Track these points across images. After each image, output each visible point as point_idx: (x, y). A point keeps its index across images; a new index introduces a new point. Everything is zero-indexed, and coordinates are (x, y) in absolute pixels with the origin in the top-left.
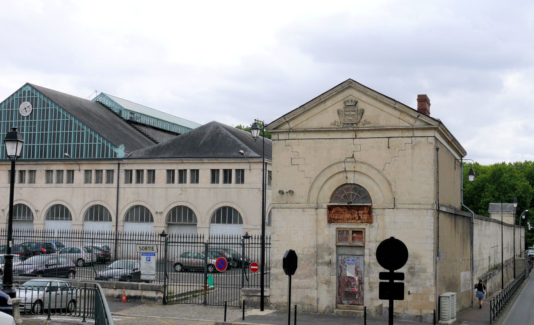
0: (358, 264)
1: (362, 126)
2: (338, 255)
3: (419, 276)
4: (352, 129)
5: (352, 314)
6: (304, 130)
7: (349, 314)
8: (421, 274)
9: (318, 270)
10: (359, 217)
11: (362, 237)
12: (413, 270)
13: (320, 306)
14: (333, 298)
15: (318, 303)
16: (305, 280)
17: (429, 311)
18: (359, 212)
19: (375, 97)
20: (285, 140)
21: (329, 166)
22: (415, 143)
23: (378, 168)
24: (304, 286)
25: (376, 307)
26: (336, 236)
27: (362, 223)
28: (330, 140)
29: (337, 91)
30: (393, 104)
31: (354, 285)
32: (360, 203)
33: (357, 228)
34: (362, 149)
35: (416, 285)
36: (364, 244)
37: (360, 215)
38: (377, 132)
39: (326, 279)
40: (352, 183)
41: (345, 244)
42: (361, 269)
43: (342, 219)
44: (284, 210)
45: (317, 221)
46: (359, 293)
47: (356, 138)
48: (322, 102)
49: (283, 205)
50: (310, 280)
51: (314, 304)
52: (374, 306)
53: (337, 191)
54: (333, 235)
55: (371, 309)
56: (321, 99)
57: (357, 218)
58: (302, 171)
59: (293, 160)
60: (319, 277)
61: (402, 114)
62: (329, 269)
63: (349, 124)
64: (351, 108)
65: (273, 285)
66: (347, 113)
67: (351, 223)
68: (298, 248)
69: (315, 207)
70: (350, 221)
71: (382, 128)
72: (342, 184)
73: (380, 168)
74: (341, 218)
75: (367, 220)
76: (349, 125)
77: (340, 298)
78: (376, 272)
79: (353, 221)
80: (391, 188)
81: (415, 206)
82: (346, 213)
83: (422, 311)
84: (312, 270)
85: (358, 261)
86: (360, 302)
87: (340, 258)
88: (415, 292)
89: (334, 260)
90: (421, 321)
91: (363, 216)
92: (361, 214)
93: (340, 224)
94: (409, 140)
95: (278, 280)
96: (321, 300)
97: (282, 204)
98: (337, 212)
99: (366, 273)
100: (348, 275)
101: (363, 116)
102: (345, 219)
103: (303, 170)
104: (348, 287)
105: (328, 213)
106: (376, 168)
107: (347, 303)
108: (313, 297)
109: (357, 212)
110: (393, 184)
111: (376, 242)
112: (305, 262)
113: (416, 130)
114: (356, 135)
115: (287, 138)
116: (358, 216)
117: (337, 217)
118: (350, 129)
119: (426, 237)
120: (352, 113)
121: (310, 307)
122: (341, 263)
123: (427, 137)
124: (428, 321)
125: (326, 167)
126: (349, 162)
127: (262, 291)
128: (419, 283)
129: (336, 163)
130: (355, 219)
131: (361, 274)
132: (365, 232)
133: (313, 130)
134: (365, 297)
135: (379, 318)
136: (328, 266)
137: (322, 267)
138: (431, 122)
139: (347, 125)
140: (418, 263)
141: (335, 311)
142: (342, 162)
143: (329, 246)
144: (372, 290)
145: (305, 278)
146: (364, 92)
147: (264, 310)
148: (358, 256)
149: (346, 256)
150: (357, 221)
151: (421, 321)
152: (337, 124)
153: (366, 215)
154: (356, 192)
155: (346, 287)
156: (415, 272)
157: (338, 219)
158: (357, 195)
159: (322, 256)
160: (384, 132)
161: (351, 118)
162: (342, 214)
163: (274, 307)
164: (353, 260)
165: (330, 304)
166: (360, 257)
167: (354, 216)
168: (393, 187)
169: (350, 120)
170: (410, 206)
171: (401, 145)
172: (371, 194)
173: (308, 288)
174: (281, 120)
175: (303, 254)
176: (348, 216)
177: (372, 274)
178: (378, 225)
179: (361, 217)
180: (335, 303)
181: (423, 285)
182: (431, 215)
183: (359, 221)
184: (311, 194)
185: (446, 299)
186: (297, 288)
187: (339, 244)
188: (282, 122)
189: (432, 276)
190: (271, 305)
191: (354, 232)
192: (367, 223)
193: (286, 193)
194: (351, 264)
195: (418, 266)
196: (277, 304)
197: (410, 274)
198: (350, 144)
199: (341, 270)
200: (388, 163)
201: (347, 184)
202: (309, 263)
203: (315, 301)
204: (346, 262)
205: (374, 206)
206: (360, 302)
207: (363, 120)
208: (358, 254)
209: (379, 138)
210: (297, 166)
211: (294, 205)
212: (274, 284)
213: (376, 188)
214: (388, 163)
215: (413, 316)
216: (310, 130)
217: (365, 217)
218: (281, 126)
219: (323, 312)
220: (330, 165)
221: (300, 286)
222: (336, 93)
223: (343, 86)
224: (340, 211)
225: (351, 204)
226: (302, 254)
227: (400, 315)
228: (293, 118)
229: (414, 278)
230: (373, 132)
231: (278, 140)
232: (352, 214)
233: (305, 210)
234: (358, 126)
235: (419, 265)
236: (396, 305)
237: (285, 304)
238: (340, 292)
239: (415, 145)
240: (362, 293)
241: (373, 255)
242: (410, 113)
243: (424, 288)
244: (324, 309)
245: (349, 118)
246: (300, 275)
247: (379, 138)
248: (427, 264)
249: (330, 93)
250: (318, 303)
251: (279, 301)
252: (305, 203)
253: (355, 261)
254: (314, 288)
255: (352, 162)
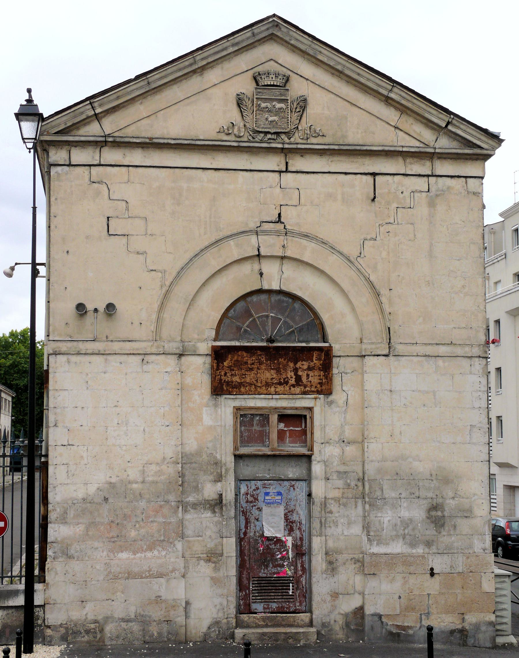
0: (293, 503)
1: (305, 142)
2: (239, 480)
3: (455, 527)
4: (280, 146)
5: (285, 640)
6: (148, 141)
7: (277, 640)
8: (460, 522)
9: (186, 523)
10: (298, 379)
11: (304, 432)
12: (439, 513)
13: (192, 622)
14: (229, 598)
15: (187, 617)
16: (149, 554)
17: (482, 615)
18: (299, 365)
19: (339, 67)
20: (90, 166)
21: (217, 242)
22: (437, 191)
23: (345, 250)
24: (149, 571)
25: (346, 615)
26: (235, 430)
27: (305, 393)
28: (217, 172)
29: (237, 44)
30: (386, 89)
31: (283, 558)
32: (295, 341)
33: (291, 408)
34: (302, 201)
35: (448, 551)
36: (311, 449)
37: (300, 373)
38: (342, 158)
39: (208, 546)
40: (275, 286)
41: (259, 450)
42: (301, 515)
43: (250, 384)
44: (88, 358)
45: (182, 388)
46: (298, 581)
47: (287, 171)
48: (194, 72)
49: (82, 347)
50: (164, 553)
51: (179, 619)
52: (340, 614)
53: (232, 311)
54: (227, 428)
55: (332, 622)
56: (195, 62)
57: (293, 381)
58: (138, 253)
59: (112, 222)
60: (189, 542)
61: (404, 117)
62: (216, 519)
63: (268, 133)
64: (276, 93)
65: (57, 574)
66: (263, 105)
67: (276, 393)
68: (129, 464)
69: (178, 351)
70: (273, 389)
71: (358, 148)
72: (249, 290)
73: (352, 251)
74: (248, 380)
75: (319, 386)
76: (269, 136)
77: (246, 598)
78: (342, 520)
79: (280, 388)
80: (380, 303)
81: (443, 350)
82: (263, 367)
83: (466, 617)
84: (170, 523)
85: (293, 494)
86: (298, 604)
87: (243, 490)
88: (448, 570)
89: (229, 496)
90: (465, 644)
91: (308, 375)
92: (304, 370)
93: (246, 396)
94: (421, 184)
95: (70, 557)
96: (195, 606)
97: (81, 343)
98: (238, 364)
99: (316, 524)
100: (267, 534)
101: (305, 115)
102: (259, 385)
103: (141, 252)
104: (267, 567)
105: (212, 367)
106: (341, 250)
107: (264, 608)
108: (174, 600)
109: (291, 365)
110: (384, 291)
111: (343, 444)
112: (149, 501)
113: (439, 158)
114: (287, 163)
115: (96, 163)
116: (296, 374)
117: (236, 379)
118: (273, 145)
119: (469, 427)
120: (278, 105)
121: (165, 629)
122: (247, 502)
123: (466, 177)
124: (482, 643)
125: (207, 244)
126: (271, 231)
127: (29, 593)
128: (455, 544)
129: (235, 235)
130: (287, 383)
131: (300, 529)
132: (312, 418)
133: (173, 142)
134: (315, 589)
135: (356, 644)
136: (214, 512)
137: (195, 516)
138: (479, 139)
139: (262, 135)
140: (451, 494)
141: (239, 632)
142: (250, 231)
143: (215, 457)
144: (333, 569)
145: (151, 548)
146: (311, 52)
147: (36, 647)
148: (293, 483)
149: (259, 483)
150: (292, 389)
151: (465, 644)
152: (236, 131)
153: (317, 373)
154: (283, 314)
155: (260, 567)
156: (444, 516)
157: (241, 384)
158: (285, 322)
159: (194, 484)
160: (360, 160)
161: (276, 118)
162: (251, 369)
163: (57, 636)
164: (279, 494)
165: (221, 615)
166: (298, 483)
167: (284, 376)
168: (384, 299)
169: (272, 122)
170: (429, 350)
171: (401, 196)
172: (325, 317)
173: (160, 575)
174: (81, 110)
175: (143, 482)
176: (268, 375)
177: (333, 528)
178: (345, 398)
179: (304, 379)
180: (233, 611)
181: (466, 551)
182: (481, 371)
183: (298, 390)
184: (166, 315)
185: (504, 582)
186: (128, 578)
187: (244, 451)
188: (84, 117)
189: (487, 527)
190: (49, 632)
191: (283, 418)
192: (319, 392)
193: (92, 312)
194: (273, 503)
195: (451, 501)
196: (67, 628)
197: (432, 522)
198: (271, 187)
199: (247, 522)
200: (372, 239)
201: (260, 291)
202: (161, 507)
203: (182, 609)
204: (261, 498)
205: (337, 349)
206: (298, 604)
207: (303, 125)
208: (291, 476)
209: (346, 174)
210: (124, 240)
211: (116, 347)
212: (58, 569)
213: (339, 303)
214: (372, 239)
215: (443, 632)
216: (166, 141)
217: (315, 378)
218: (78, 129)
219: (201, 639)
220: (218, 238)
221: (136, 570)
222: (236, 48)
223: (256, 31)
224: (246, 363)
225: (275, 344)
226: (140, 479)
227: (411, 632)
228: (114, 108)
229: (444, 533)
230: (332, 158)
231: (70, 165)
232: (278, 371)
233: (147, 358)
234: (292, 140)
235: (453, 498)
236: (400, 606)
237: (93, 626)
238: (245, 582)
239: (437, 196)
240: (303, 580)
241: (335, 477)
242: (427, 115)
243: (468, 558)
244: (204, 630)
245: (271, 119)
246: (135, 541)
247: (346, 174)
248: (474, 495)
249: (220, 48)
250: (187, 617)
251: (74, 618)
252: (149, 341)
253: (285, 495)
254: (177, 574)
255: (278, 233)
